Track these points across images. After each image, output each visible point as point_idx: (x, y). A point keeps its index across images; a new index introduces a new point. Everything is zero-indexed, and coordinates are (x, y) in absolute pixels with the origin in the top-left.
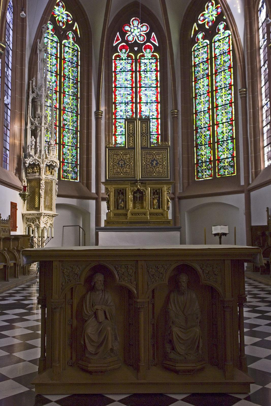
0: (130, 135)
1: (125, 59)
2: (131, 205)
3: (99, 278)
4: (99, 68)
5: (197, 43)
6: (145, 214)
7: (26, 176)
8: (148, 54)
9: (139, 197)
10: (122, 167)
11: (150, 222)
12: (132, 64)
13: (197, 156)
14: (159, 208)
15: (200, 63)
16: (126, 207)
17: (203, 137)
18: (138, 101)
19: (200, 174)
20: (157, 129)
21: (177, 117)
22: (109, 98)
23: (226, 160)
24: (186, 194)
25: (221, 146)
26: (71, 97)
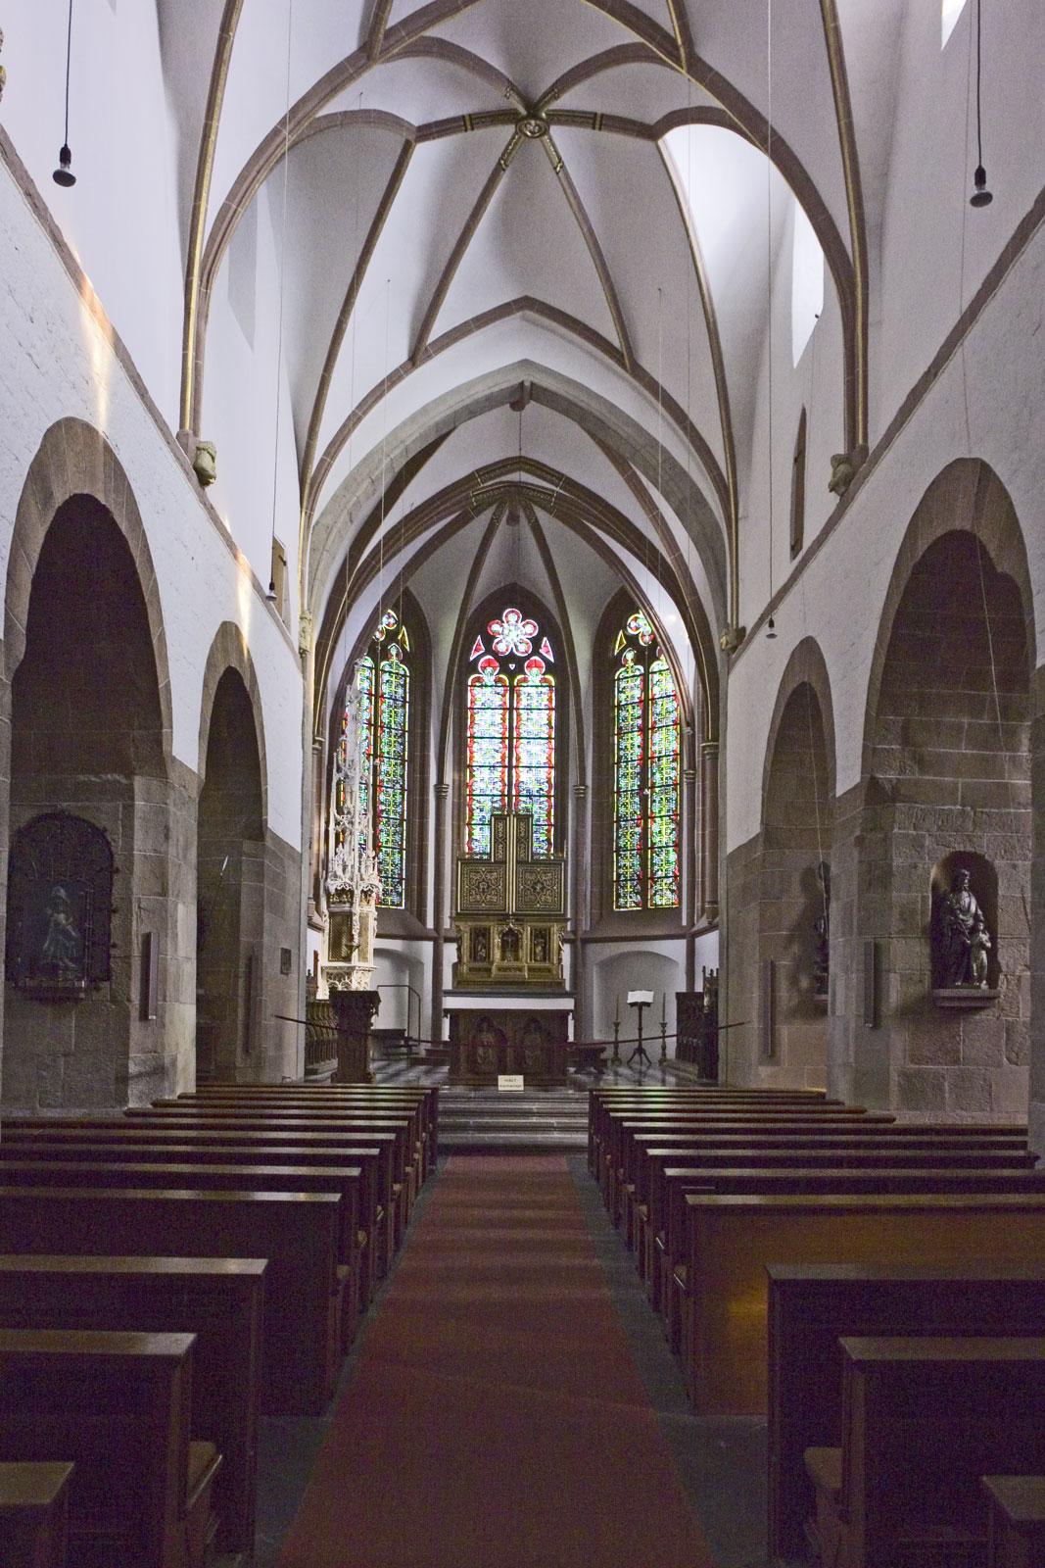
0: (499, 840)
1: (491, 686)
2: (497, 954)
3: (485, 1025)
4: (444, 708)
5: (624, 666)
6: (520, 969)
7: (328, 907)
8: (534, 675)
9: (511, 942)
10: (483, 892)
11: (528, 983)
12: (504, 696)
13: (619, 867)
14: (544, 959)
15: (627, 704)
16: (489, 958)
17: (628, 837)
18: (514, 763)
19: (622, 901)
20: (549, 815)
21: (584, 798)
22: (460, 759)
23: (665, 880)
24: (598, 935)
25: (658, 855)
26: (393, 762)
